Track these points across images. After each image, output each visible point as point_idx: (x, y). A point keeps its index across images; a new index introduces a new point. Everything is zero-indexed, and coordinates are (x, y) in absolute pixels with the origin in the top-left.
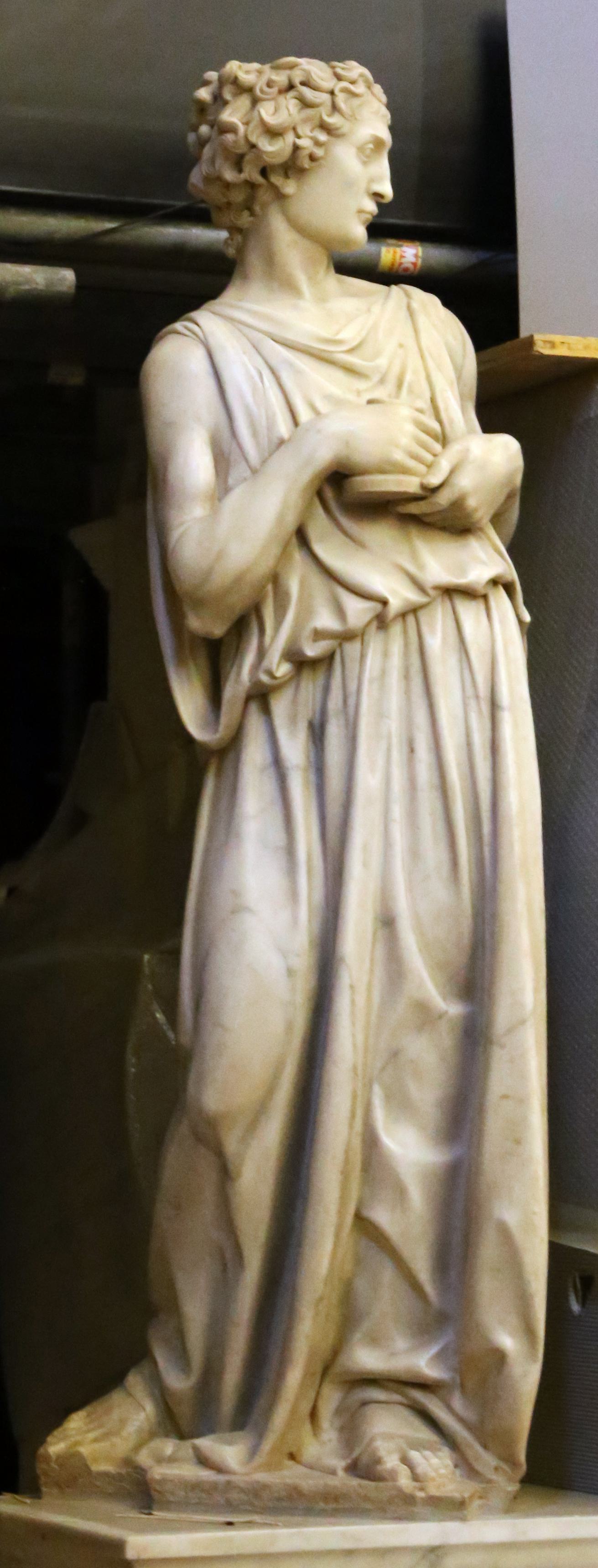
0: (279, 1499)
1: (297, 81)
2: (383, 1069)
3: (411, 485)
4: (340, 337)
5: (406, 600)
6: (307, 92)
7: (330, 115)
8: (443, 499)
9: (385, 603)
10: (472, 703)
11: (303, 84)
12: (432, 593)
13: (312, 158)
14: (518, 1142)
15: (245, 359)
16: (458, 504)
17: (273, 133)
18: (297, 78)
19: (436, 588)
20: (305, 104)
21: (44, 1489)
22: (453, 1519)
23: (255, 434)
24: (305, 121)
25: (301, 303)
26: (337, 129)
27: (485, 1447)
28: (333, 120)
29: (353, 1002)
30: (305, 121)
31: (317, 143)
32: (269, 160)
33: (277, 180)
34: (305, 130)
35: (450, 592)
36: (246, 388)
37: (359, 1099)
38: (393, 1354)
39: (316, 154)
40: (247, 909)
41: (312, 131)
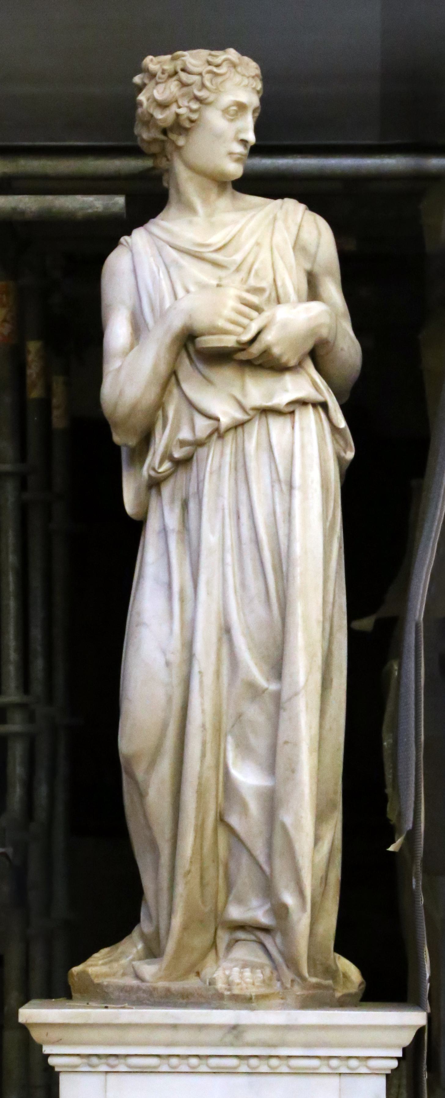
0: (161, 997)
1: (178, 69)
2: (233, 726)
3: (229, 341)
4: (208, 242)
5: (234, 418)
6: (183, 76)
7: (200, 90)
8: (256, 349)
9: (217, 420)
10: (277, 486)
11: (183, 70)
12: (251, 413)
13: (192, 121)
14: (293, 771)
15: (152, 260)
16: (266, 352)
17: (163, 106)
18: (179, 65)
19: (255, 409)
20: (184, 85)
21: (73, 994)
22: (247, 1008)
23: (153, 310)
24: (183, 96)
25: (195, 219)
26: (206, 99)
27: (288, 967)
28: (202, 94)
29: (201, 683)
30: (183, 96)
31: (192, 111)
32: (163, 125)
33: (173, 136)
34: (184, 102)
35: (266, 411)
36: (149, 282)
37: (208, 746)
38: (249, 909)
39: (192, 118)
40: (144, 624)
41: (189, 102)
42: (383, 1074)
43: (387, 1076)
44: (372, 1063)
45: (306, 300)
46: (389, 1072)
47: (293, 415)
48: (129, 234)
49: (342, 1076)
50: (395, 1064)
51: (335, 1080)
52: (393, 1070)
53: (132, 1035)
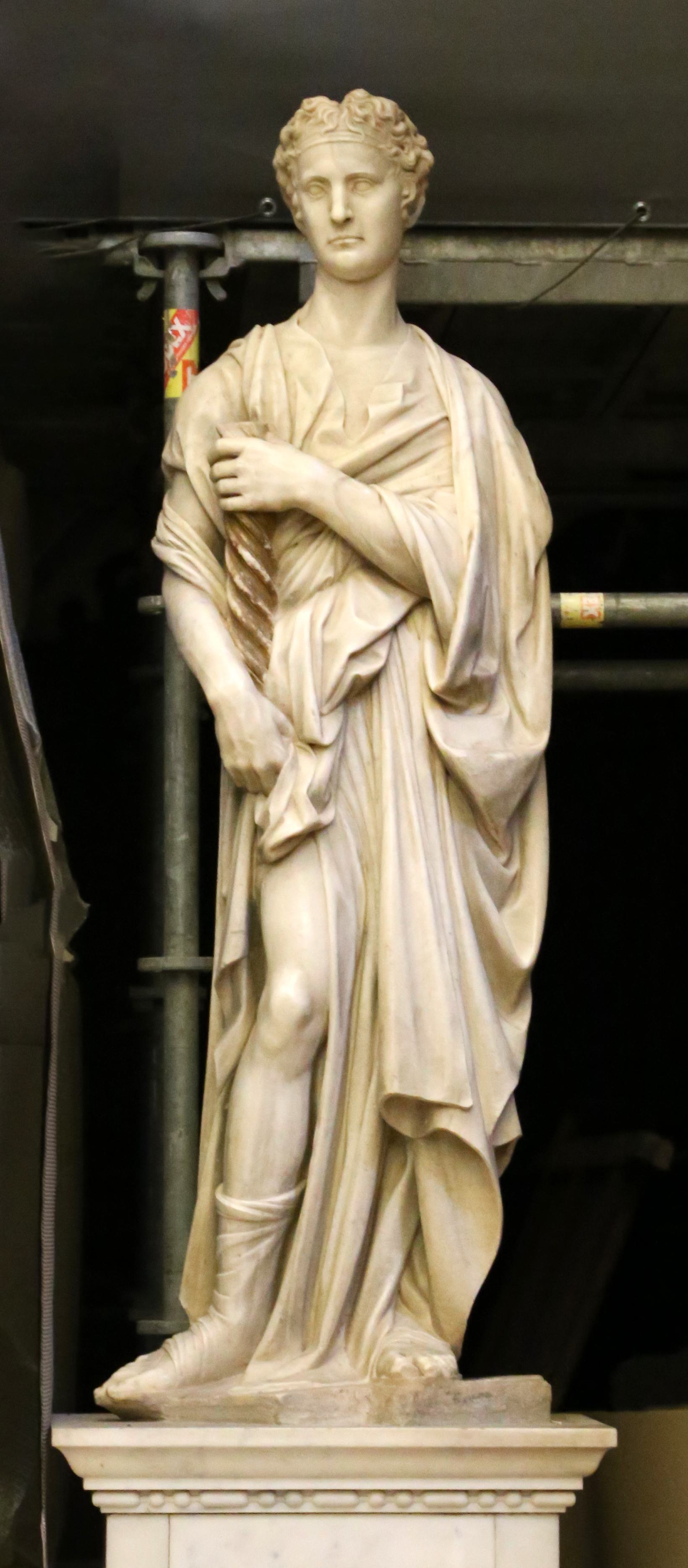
42: (552, 1514)
43: (561, 1516)
44: (539, 1499)
45: (303, 270)
46: (563, 1511)
47: (553, 606)
48: (263, 324)
49: (171, 1517)
50: (571, 1500)
51: (488, 1521)
52: (569, 1509)
53: (215, 1464)
